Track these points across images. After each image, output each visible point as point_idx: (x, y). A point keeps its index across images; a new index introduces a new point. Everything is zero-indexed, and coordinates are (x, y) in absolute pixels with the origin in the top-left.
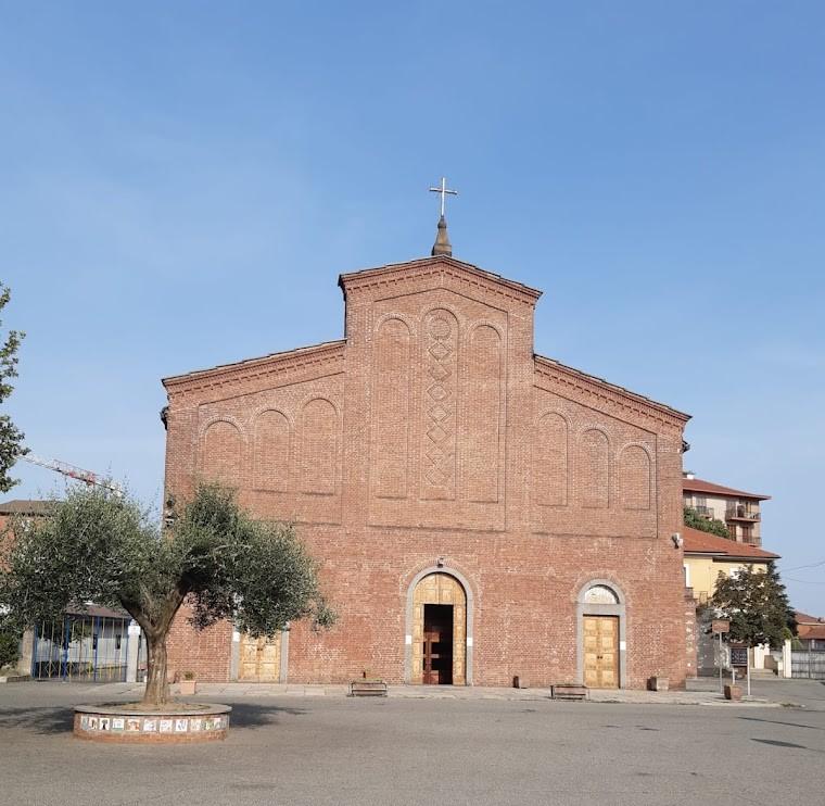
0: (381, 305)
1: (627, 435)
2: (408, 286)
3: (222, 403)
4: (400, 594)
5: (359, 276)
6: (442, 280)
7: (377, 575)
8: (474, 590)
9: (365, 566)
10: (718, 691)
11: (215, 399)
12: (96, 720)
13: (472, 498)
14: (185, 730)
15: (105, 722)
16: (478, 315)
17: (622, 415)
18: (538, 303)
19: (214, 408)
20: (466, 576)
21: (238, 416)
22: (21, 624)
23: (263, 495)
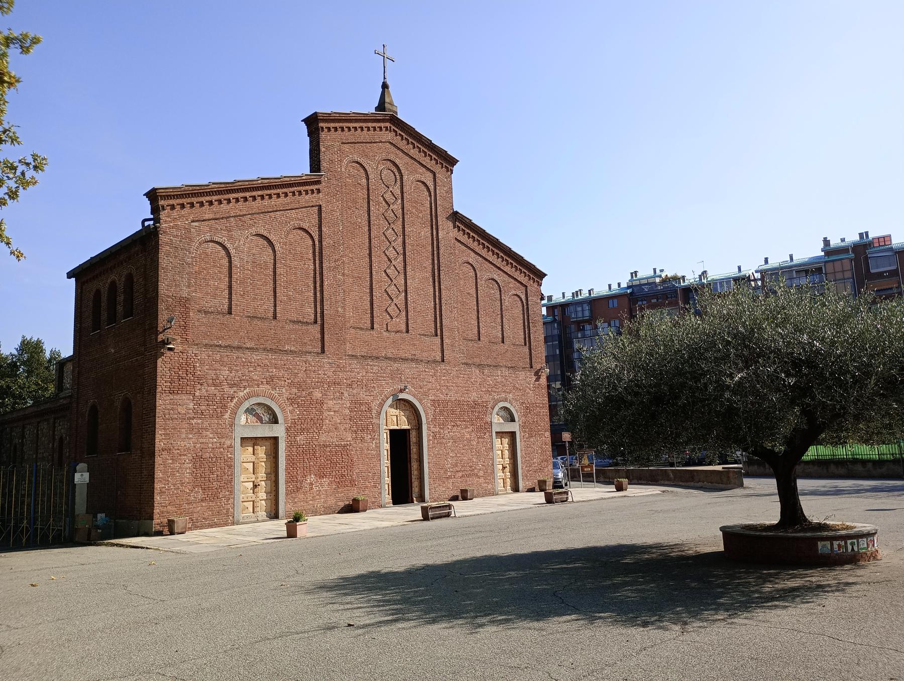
0: (346, 147)
1: (511, 285)
2: (365, 135)
3: (213, 222)
4: (374, 421)
5: (330, 118)
6: (390, 136)
7: (356, 403)
8: (427, 414)
9: (346, 395)
10: (814, 448)
11: (207, 216)
12: (843, 543)
13: (420, 331)
14: (860, 540)
15: (852, 544)
16: (417, 172)
17: (507, 269)
18: (455, 168)
19: (204, 227)
20: (420, 401)
21: (230, 238)
22: (757, 283)
23: (255, 322)
